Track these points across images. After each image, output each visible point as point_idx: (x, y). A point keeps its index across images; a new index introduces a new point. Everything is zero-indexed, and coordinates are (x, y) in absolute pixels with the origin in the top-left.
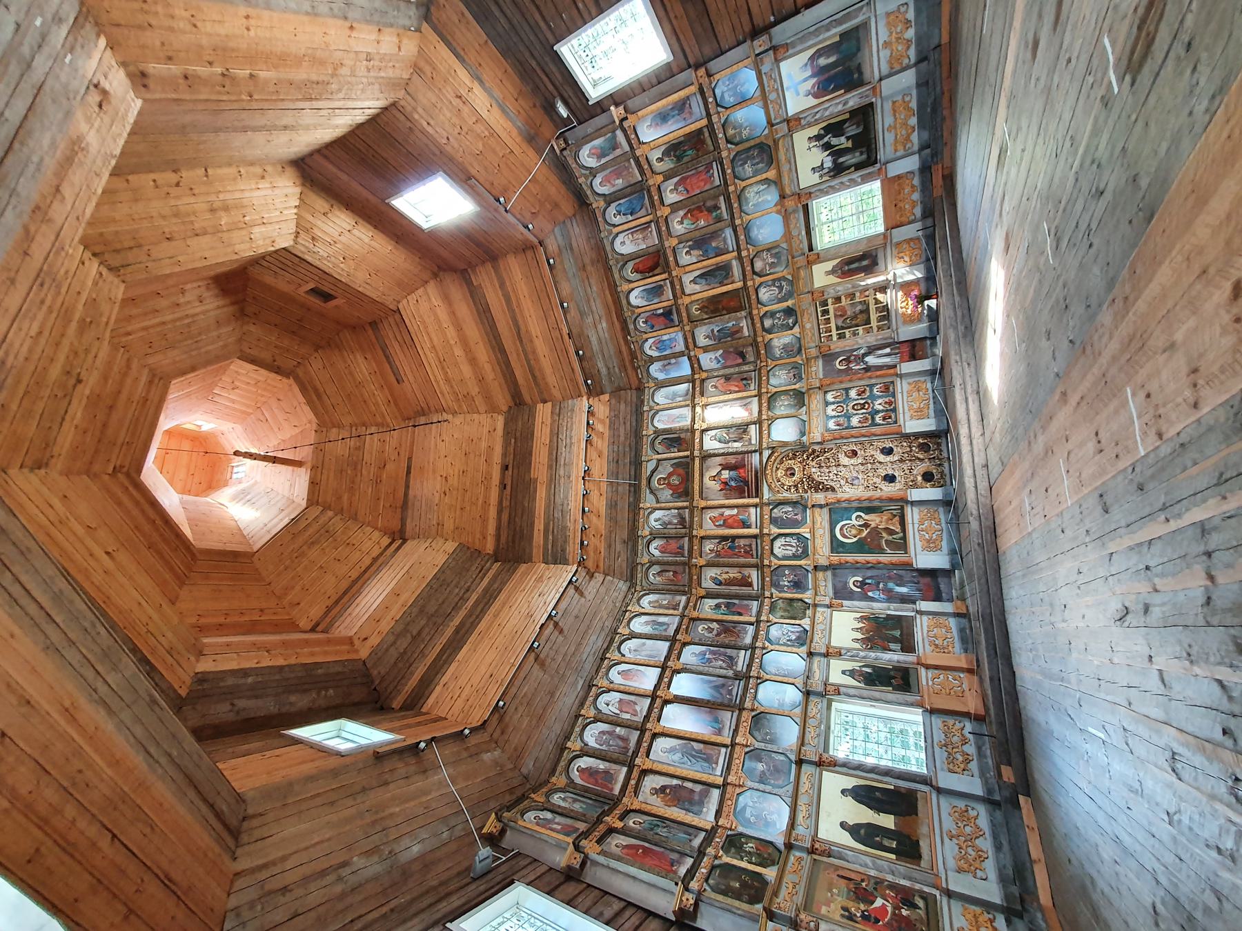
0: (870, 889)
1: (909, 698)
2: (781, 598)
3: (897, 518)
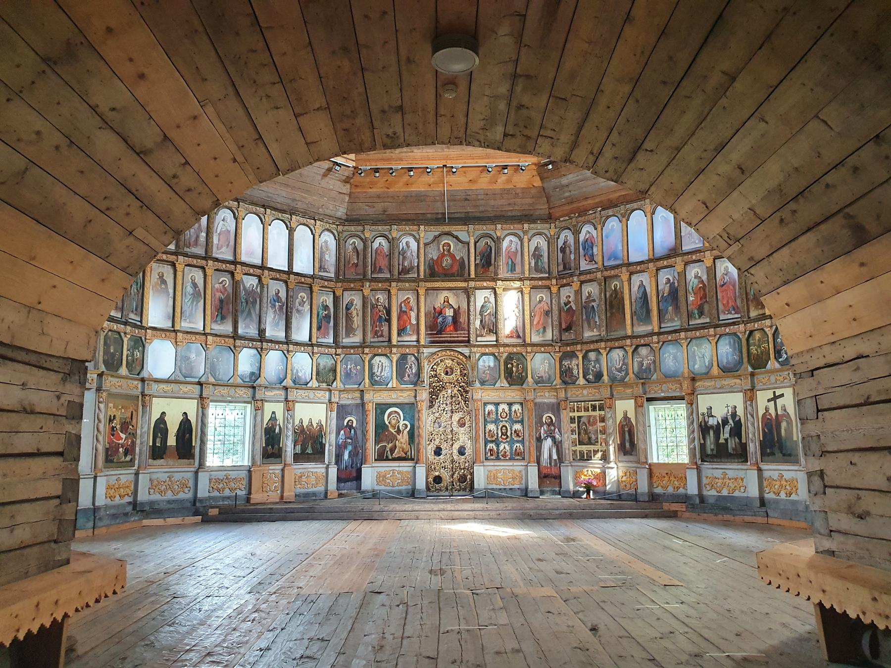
0: (129, 431)
1: (258, 457)
2: (336, 362)
3: (404, 455)
